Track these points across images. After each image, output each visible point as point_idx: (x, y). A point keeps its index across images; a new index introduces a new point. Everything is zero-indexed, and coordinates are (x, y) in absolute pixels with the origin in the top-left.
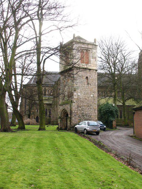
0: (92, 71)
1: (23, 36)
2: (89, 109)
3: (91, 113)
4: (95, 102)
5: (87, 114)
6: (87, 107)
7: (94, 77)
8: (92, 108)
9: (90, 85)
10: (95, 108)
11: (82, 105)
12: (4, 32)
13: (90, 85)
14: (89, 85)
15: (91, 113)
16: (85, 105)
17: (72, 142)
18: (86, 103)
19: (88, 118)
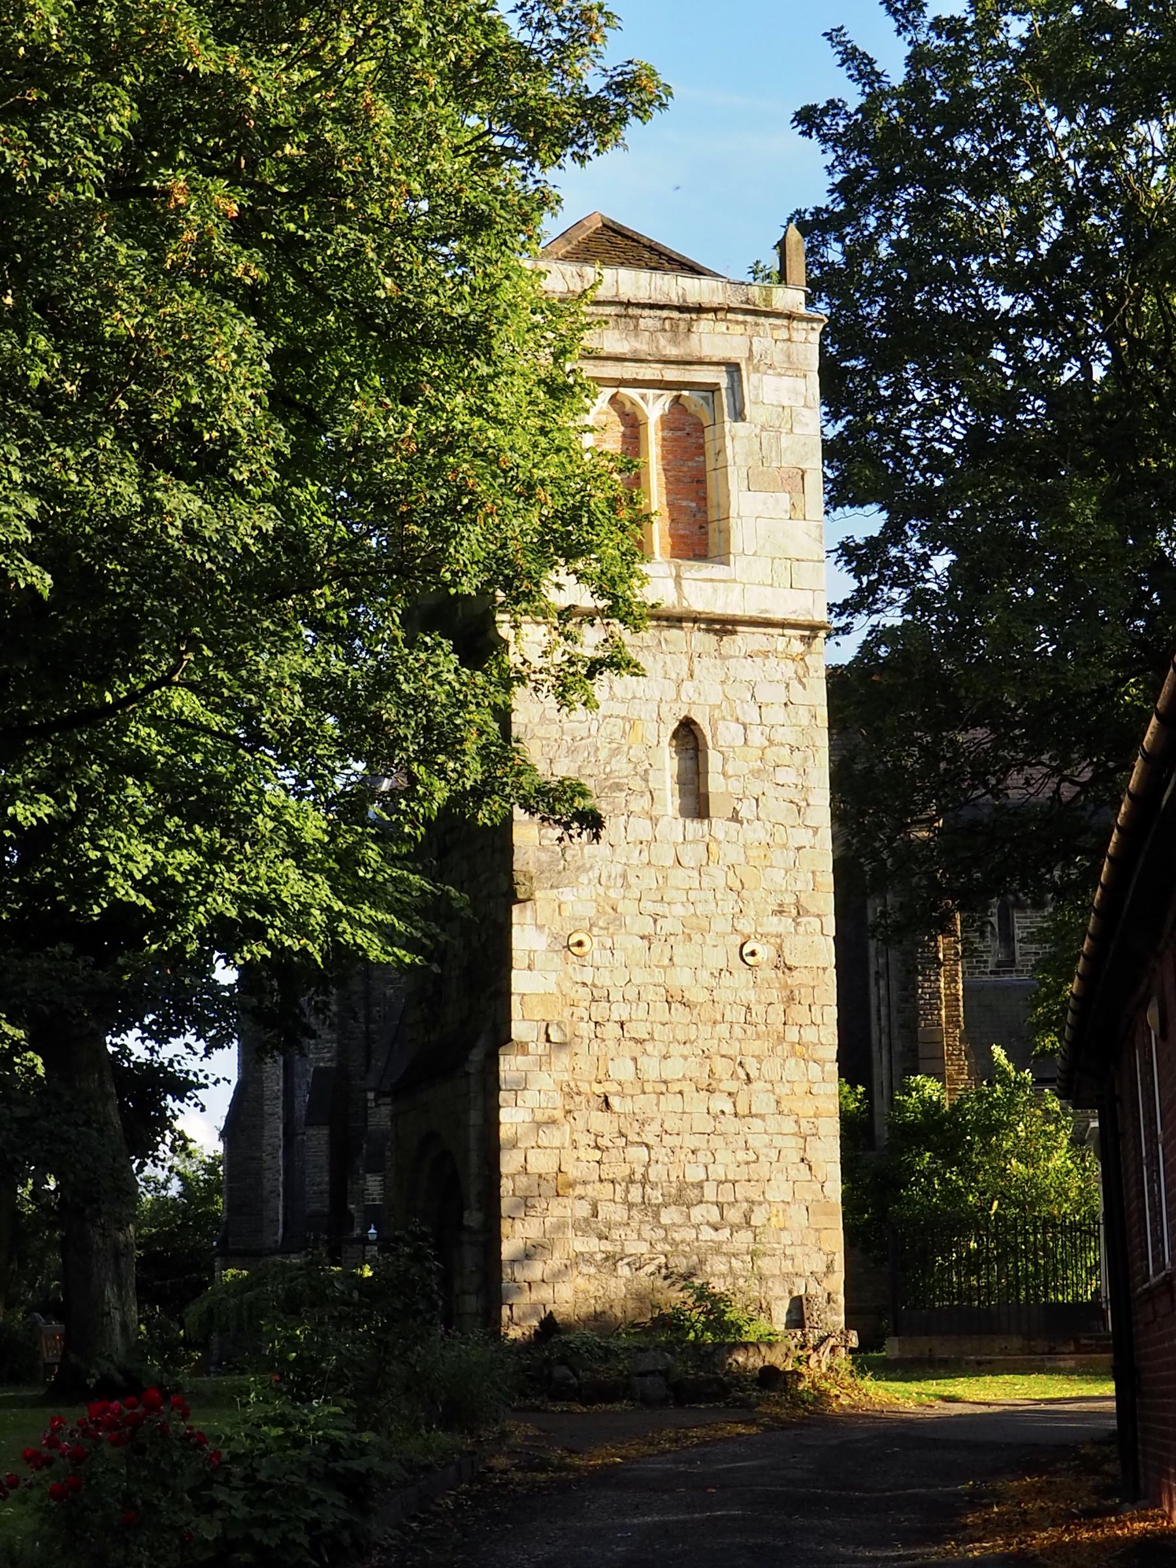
0: (746, 639)
1: (601, 1181)
2: (730, 1125)
3: (763, 1170)
4: (809, 1034)
5: (700, 1185)
6: (697, 1103)
7: (775, 715)
8: (763, 1102)
9: (735, 818)
10: (806, 1108)
11: (623, 1070)
12: (400, 961)
13: (735, 818)
14: (719, 826)
15: (763, 1170)
16: (674, 1069)
17: (303, 86)
18: (676, 1049)
19: (707, 1234)
